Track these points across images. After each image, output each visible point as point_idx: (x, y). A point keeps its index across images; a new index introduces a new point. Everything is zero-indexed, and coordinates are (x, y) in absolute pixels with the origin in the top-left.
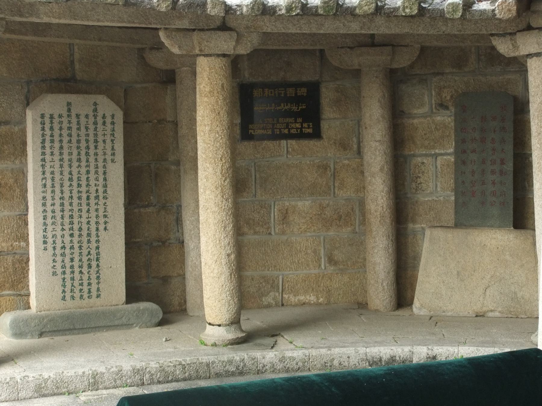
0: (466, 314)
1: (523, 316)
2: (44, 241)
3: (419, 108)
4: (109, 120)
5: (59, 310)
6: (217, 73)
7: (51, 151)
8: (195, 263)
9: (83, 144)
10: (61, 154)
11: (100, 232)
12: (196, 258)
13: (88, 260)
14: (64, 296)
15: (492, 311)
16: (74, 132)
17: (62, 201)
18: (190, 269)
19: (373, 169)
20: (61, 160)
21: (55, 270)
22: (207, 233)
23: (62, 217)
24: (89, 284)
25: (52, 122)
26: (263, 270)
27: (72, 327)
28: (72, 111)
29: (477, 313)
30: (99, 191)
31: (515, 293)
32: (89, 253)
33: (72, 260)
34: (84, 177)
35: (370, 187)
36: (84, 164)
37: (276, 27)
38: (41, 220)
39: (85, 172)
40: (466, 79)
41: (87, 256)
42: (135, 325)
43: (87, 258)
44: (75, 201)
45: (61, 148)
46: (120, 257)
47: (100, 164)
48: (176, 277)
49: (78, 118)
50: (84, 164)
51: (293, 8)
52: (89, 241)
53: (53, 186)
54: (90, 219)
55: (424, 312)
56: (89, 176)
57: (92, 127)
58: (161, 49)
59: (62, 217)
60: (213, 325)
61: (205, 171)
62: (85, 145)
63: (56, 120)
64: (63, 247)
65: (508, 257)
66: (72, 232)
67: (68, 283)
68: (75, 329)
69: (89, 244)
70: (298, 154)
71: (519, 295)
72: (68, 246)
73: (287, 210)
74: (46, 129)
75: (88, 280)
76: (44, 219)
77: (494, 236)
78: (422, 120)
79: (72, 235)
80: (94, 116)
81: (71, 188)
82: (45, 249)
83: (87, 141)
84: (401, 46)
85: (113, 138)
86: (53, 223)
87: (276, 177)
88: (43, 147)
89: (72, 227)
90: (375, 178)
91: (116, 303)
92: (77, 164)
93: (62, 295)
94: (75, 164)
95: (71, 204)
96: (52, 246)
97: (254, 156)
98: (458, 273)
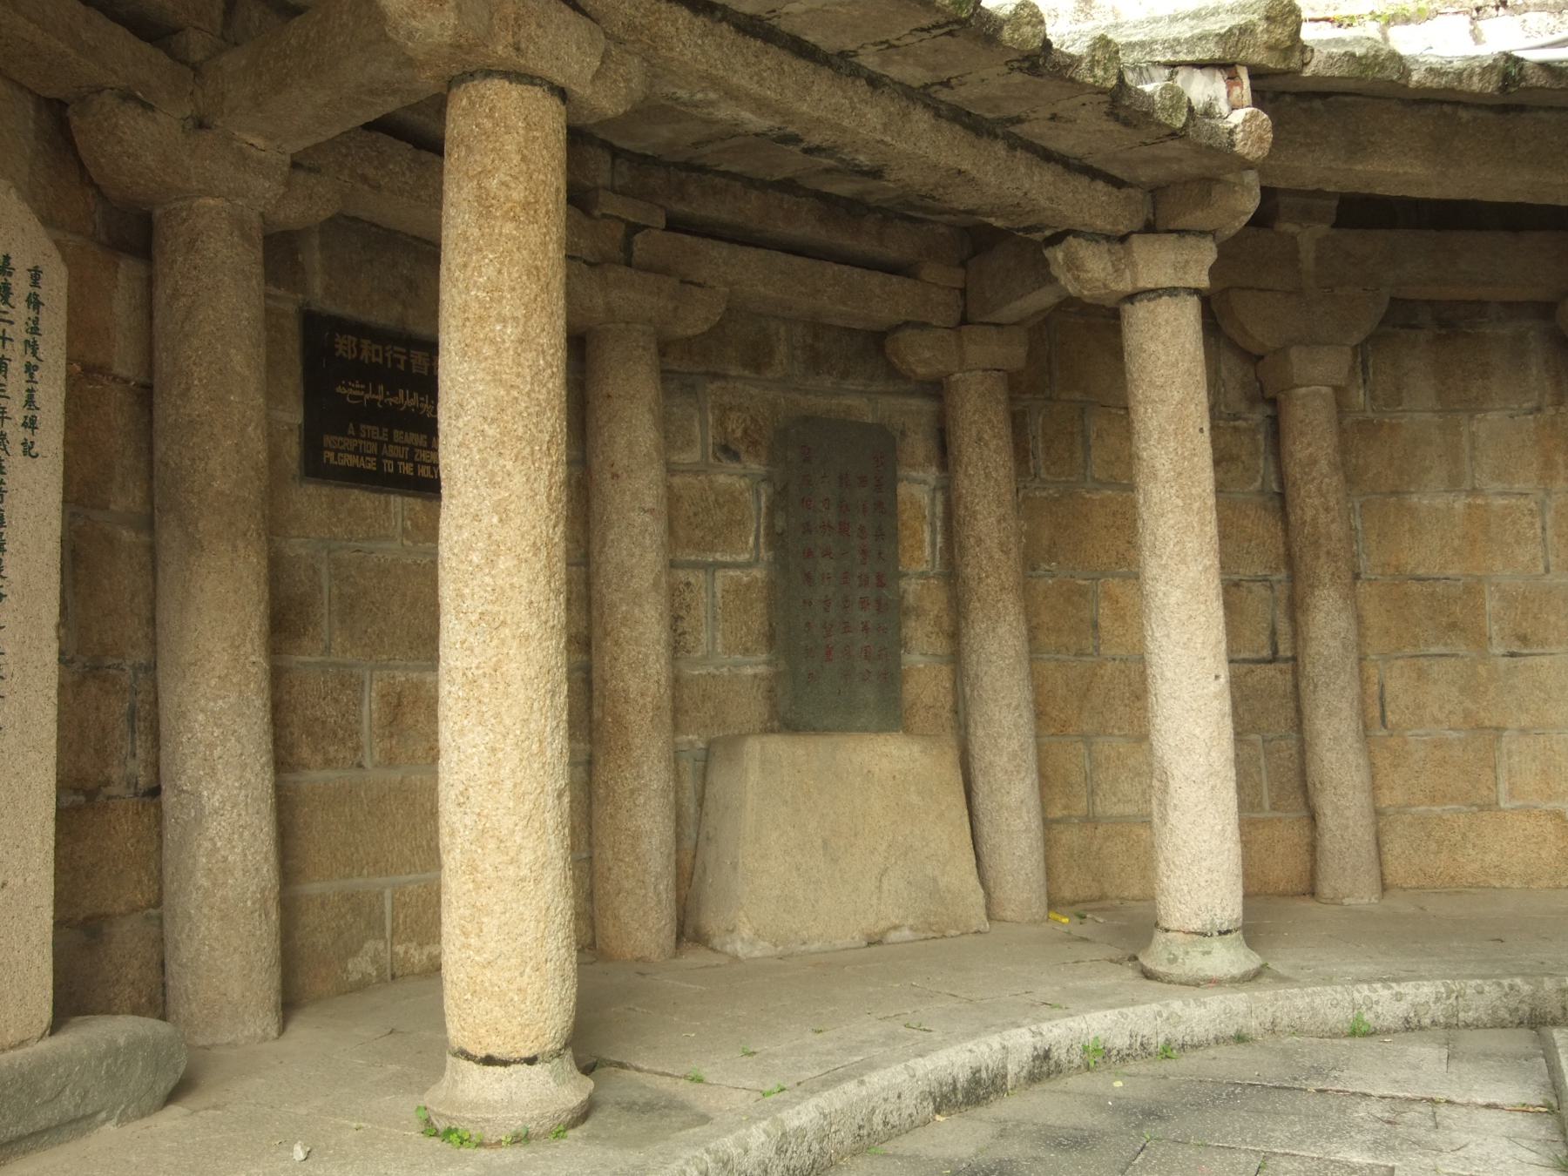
1: (953, 932)
6: (546, 147)
8: (225, 859)
12: (230, 841)
15: (896, 928)
18: (205, 883)
19: (635, 584)
22: (497, 715)
26: (350, 876)
29: (869, 935)
31: (935, 880)
37: (704, 53)
42: (103, 1115)
46: (37, 840)
48: (122, 915)
55: (762, 949)
58: (152, 108)
60: (505, 1063)
61: (493, 484)
71: (943, 882)
73: (400, 694)
77: (885, 749)
78: (689, 479)
84: (691, 283)
85: (33, 361)
87: (378, 597)
91: (19, 1037)
97: (330, 530)
98: (825, 843)
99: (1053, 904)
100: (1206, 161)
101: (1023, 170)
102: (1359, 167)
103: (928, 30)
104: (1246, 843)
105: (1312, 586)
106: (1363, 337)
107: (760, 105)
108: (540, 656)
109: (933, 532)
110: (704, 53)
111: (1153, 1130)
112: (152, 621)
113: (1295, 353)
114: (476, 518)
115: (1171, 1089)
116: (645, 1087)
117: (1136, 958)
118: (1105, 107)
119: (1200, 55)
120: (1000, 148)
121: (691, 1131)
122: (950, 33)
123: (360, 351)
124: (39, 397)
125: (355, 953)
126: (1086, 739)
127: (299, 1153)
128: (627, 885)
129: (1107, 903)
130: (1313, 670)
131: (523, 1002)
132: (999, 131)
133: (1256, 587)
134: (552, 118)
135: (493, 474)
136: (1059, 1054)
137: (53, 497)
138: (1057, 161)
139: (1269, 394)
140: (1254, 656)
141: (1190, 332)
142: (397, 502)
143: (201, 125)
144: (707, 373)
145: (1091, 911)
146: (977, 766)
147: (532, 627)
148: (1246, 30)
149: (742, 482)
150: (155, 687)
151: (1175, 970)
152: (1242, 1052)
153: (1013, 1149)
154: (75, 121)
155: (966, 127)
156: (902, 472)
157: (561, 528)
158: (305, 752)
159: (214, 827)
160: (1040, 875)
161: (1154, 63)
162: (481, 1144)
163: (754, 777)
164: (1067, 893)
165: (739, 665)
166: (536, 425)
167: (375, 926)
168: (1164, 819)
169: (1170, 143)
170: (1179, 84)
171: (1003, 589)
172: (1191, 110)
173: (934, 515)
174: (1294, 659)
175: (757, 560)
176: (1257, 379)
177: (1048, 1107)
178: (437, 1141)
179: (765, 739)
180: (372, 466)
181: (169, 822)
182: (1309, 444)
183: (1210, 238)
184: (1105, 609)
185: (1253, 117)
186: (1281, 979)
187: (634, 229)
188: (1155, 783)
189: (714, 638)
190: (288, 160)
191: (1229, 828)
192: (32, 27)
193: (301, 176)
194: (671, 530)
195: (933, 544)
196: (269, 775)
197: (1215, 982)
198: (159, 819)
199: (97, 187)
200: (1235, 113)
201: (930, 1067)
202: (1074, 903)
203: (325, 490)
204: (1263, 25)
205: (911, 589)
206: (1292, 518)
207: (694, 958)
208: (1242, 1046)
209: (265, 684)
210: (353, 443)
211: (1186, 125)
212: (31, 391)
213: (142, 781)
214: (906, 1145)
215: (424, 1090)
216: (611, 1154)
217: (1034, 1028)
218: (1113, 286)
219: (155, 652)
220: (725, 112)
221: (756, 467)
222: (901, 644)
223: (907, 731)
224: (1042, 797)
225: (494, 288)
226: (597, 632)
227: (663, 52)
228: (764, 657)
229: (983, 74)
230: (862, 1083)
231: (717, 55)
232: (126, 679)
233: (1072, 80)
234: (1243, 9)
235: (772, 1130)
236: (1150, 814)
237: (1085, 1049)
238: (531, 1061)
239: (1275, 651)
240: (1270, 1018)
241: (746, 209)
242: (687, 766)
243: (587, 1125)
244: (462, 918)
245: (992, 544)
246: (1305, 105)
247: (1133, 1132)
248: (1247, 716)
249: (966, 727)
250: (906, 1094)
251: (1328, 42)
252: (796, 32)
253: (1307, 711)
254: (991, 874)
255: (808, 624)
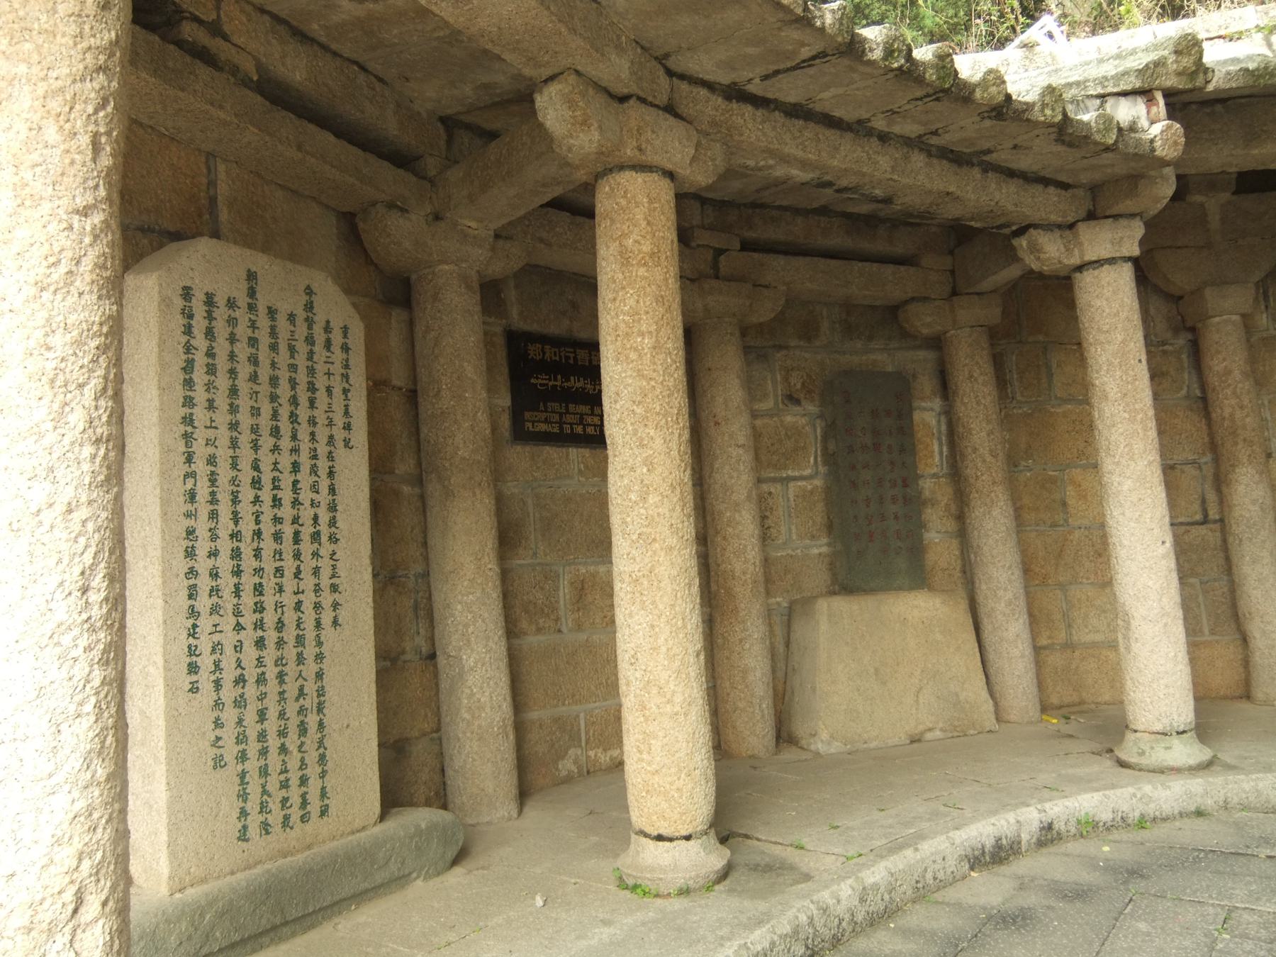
0: (896, 741)
1: (972, 732)
2: (190, 664)
3: (760, 401)
4: (337, 338)
5: (232, 873)
7: (206, 396)
8: (479, 700)
9: (284, 391)
10: (233, 409)
11: (323, 632)
13: (299, 713)
14: (245, 827)
15: (930, 730)
16: (264, 354)
17: (236, 544)
18: (467, 716)
20: (234, 426)
21: (219, 752)
22: (653, 603)
23: (237, 592)
24: (304, 781)
25: (210, 316)
26: (556, 706)
27: (278, 921)
28: (258, 295)
30: (320, 521)
32: (301, 693)
33: (262, 716)
34: (287, 480)
35: (730, 530)
36: (286, 443)
37: (765, 134)
38: (182, 601)
39: (289, 468)
40: (819, 357)
41: (297, 699)
42: (414, 875)
43: (296, 707)
44: (268, 545)
45: (234, 391)
47: (322, 449)
48: (417, 738)
49: (273, 319)
50: (286, 443)
51: (893, 51)
52: (300, 659)
53: (213, 500)
54: (301, 597)
55: (836, 747)
56: (299, 477)
57: (302, 348)
58: (407, 211)
59: (237, 592)
60: (671, 840)
61: (642, 446)
62: (289, 394)
63: (221, 313)
64: (240, 681)
65: (939, 637)
66: (260, 633)
67: (254, 789)
68: (286, 923)
69: (301, 667)
70: (594, 476)
72: (251, 674)
74: (195, 331)
75: (300, 768)
76: (190, 597)
77: (916, 603)
79: (260, 643)
80: (307, 319)
81: (257, 507)
82: (194, 689)
83: (293, 383)
85: (347, 386)
86: (215, 610)
88: (189, 383)
89: (261, 621)
90: (739, 512)
92: (272, 441)
93: (239, 826)
94: (267, 442)
95: (257, 554)
96: (213, 678)
98: (876, 670)
99: (1044, 709)
100: (1133, 164)
101: (993, 186)
102: (1255, 152)
103: (921, 99)
104: (1193, 661)
105: (1233, 465)
106: (1263, 274)
107: (804, 164)
108: (680, 561)
109: (941, 445)
110: (765, 134)
111: (1137, 886)
112: (425, 544)
113: (1208, 292)
114: (632, 469)
115: (1148, 853)
116: (763, 853)
117: (1111, 751)
118: (1053, 137)
119: (1124, 87)
120: (976, 172)
121: (800, 886)
122: (937, 99)
123: (544, 353)
124: (352, 410)
125: (563, 758)
126: (1062, 587)
127: (539, 902)
128: (741, 705)
129: (1085, 707)
130: (1238, 529)
131: (681, 797)
132: (975, 160)
133: (1188, 468)
134: (664, 191)
135: (642, 439)
136: (1059, 826)
137: (363, 473)
138: (1018, 177)
139: (1189, 324)
140: (1189, 520)
141: (1127, 289)
142: (574, 453)
143: (437, 217)
144: (774, 346)
145: (1074, 713)
146: (983, 611)
147: (673, 541)
148: (1158, 64)
149: (803, 420)
150: (429, 587)
151: (1144, 761)
152: (1199, 823)
153: (1031, 899)
154: (361, 225)
155: (951, 161)
156: (915, 404)
157: (688, 472)
158: (524, 624)
159: (471, 679)
160: (1034, 689)
161: (1088, 97)
162: (657, 896)
163: (824, 626)
164: (1055, 700)
165: (810, 548)
166: (668, 403)
167: (574, 738)
168: (1128, 649)
169: (1105, 155)
170: (1108, 110)
171: (994, 483)
172: (1120, 130)
173: (940, 432)
174: (1222, 520)
175: (817, 473)
176: (1179, 313)
177: (1052, 866)
178: (627, 892)
179: (830, 599)
180: (556, 430)
181: (443, 676)
182: (1224, 360)
183: (1138, 218)
184: (1070, 491)
185: (1169, 127)
186: (1230, 768)
187: (719, 252)
188: (1120, 622)
189: (790, 529)
190: (492, 233)
191: (1180, 655)
192: (333, 170)
193: (501, 242)
194: (757, 458)
195: (941, 453)
196: (503, 642)
197: (1176, 770)
198: (436, 675)
199: (376, 265)
200: (1155, 127)
201: (965, 837)
202: (1061, 707)
203: (528, 448)
204: (1172, 58)
205: (926, 486)
206: (1214, 415)
207: (789, 754)
208: (1201, 819)
209: (498, 583)
210: (543, 416)
211: (1116, 141)
212: (346, 406)
213: (424, 650)
214: (951, 894)
215: (616, 856)
216: (746, 903)
217: (1039, 807)
218: (1066, 261)
219: (428, 565)
220: (780, 172)
221: (812, 408)
222: (922, 526)
223: (931, 588)
224: (1032, 631)
225: (634, 313)
226: (711, 532)
227: (736, 138)
228: (825, 541)
229: (962, 123)
230: (917, 850)
231: (772, 134)
232: (411, 584)
233: (1028, 120)
234: (1156, 47)
235: (855, 885)
236: (1116, 640)
237: (1079, 822)
238: (688, 838)
239: (1206, 515)
240: (1222, 798)
241: (796, 230)
242: (776, 619)
243: (727, 882)
244: (638, 740)
245: (984, 451)
246: (1208, 110)
247: (1122, 887)
248: (1186, 565)
249: (973, 583)
250: (949, 858)
251: (1225, 62)
252: (826, 110)
253: (1235, 559)
254: (997, 688)
255: (855, 517)
